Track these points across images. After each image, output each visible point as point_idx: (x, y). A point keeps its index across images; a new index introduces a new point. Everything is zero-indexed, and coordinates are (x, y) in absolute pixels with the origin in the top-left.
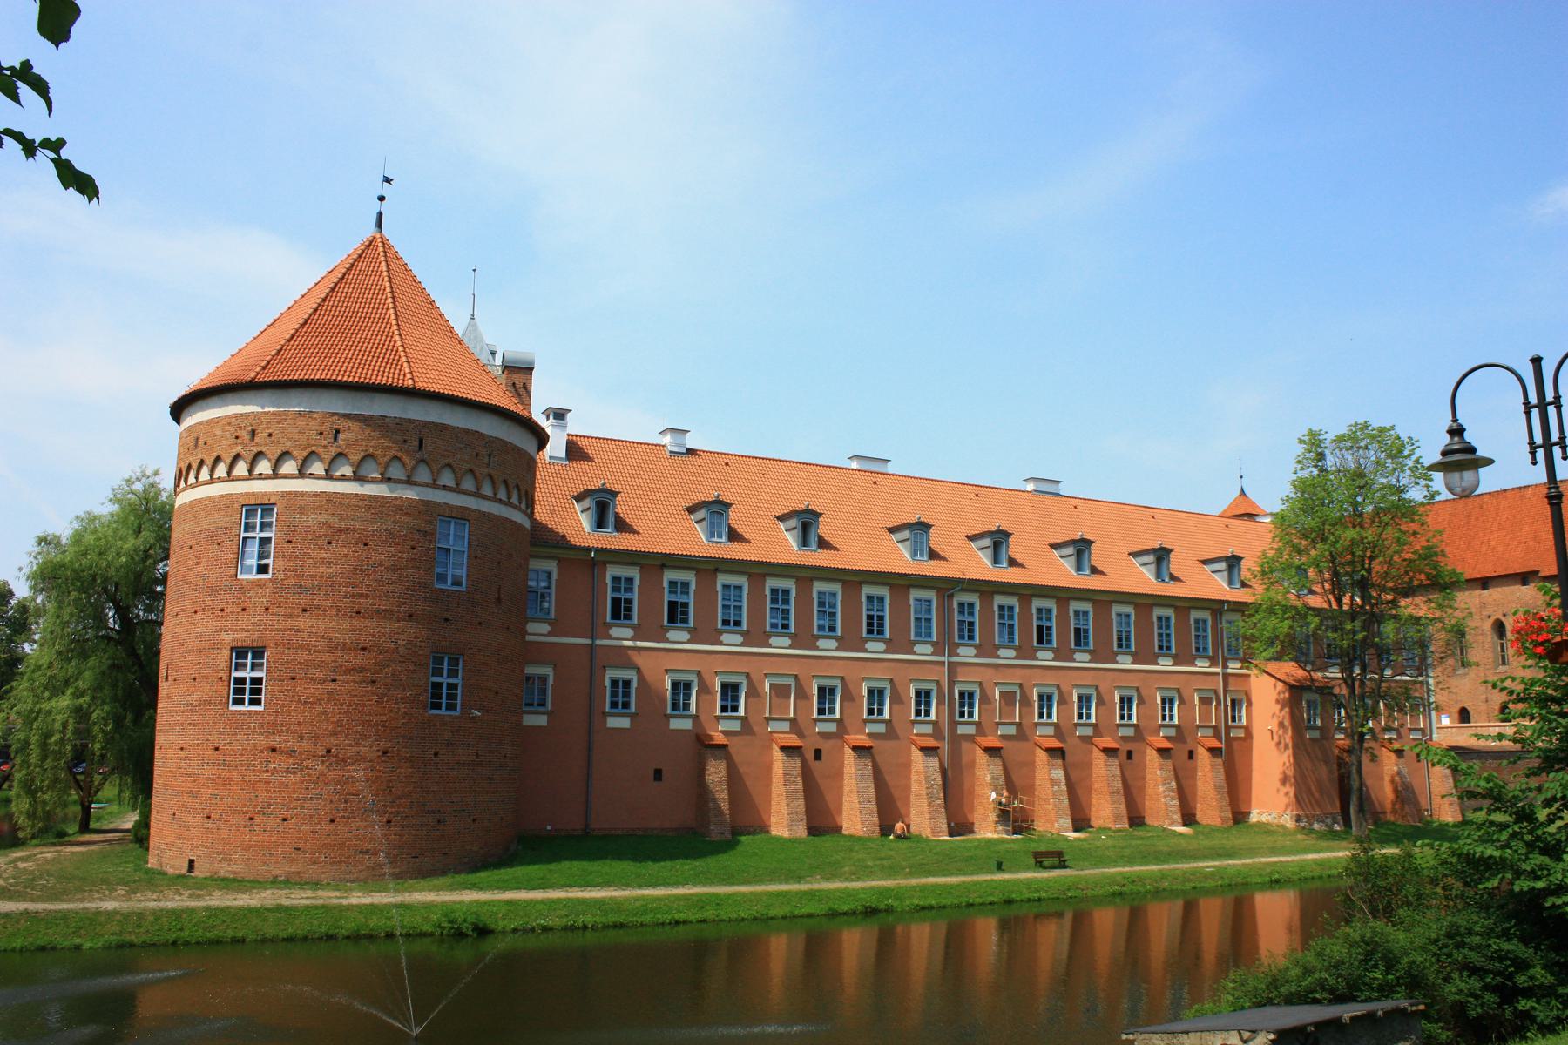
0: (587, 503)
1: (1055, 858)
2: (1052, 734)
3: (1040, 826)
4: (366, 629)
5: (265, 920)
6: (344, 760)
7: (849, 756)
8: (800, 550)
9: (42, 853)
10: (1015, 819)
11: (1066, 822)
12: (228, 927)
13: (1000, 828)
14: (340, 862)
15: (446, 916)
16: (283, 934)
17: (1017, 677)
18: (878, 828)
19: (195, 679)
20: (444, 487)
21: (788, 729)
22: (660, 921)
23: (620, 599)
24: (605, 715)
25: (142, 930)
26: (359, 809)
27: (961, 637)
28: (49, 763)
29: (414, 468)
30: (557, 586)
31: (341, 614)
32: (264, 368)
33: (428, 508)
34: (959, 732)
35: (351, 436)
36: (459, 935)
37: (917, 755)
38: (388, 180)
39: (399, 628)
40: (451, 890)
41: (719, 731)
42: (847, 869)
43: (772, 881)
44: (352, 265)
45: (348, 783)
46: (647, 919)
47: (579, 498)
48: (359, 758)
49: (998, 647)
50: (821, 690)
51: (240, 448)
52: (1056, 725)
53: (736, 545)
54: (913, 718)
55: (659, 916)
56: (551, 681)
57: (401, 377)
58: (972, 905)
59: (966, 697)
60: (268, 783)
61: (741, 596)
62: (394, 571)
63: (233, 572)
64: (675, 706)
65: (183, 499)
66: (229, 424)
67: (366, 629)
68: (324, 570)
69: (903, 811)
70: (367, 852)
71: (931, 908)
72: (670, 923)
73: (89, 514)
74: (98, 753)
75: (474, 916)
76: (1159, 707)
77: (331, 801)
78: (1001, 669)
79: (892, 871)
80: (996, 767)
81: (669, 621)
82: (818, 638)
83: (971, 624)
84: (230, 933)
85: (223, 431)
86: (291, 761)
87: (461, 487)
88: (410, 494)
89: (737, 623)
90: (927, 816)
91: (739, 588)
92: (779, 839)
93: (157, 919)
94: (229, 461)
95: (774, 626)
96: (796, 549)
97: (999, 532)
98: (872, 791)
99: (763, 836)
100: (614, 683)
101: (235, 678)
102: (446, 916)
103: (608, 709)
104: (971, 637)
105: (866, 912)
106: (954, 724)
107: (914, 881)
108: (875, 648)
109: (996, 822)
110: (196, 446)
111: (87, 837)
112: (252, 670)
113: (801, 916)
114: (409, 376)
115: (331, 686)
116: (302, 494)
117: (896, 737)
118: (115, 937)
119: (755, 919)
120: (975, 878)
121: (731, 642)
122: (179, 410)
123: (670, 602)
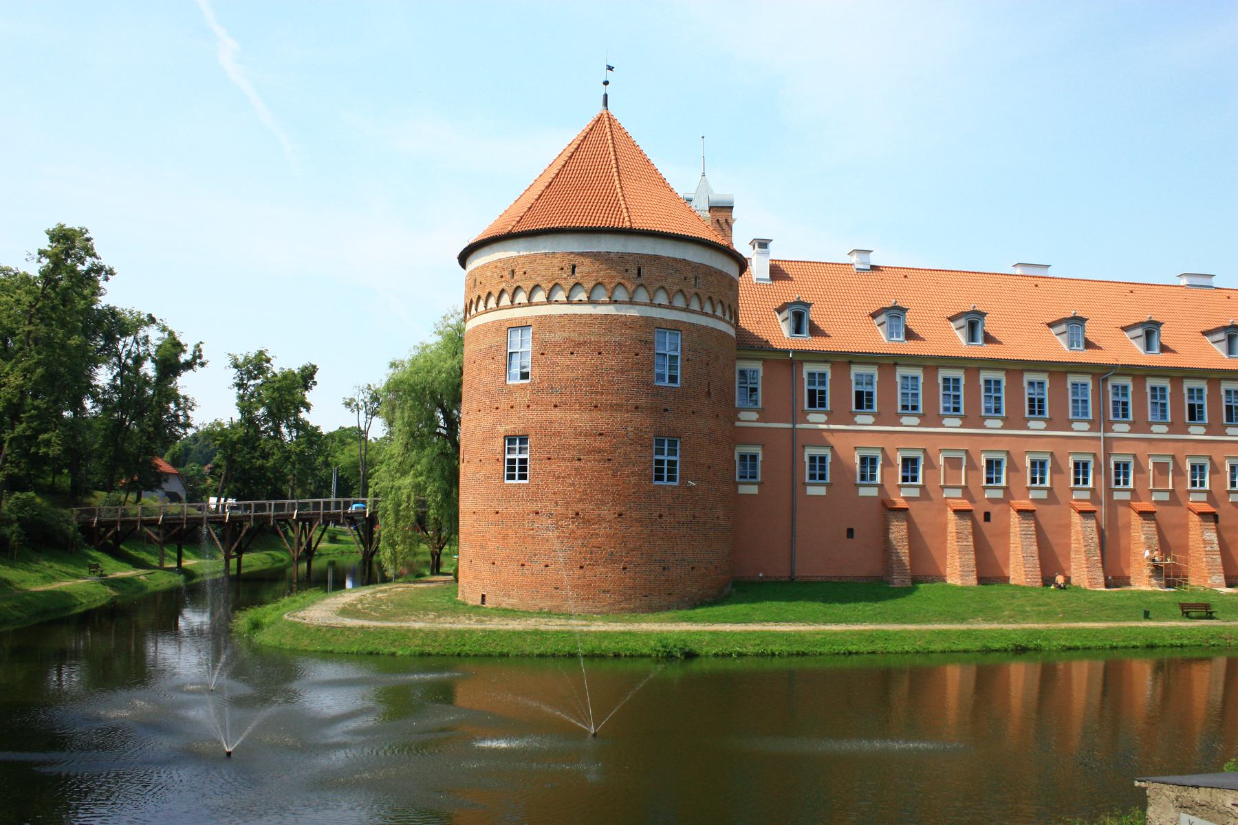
0: (786, 313)
1: (1206, 611)
2: (1205, 499)
3: (1193, 581)
4: (603, 419)
5: (525, 640)
6: (588, 521)
7: (1015, 518)
8: (968, 345)
9: (397, 588)
10: (1170, 575)
11: (1220, 579)
12: (497, 644)
13: (1154, 581)
14: (588, 599)
15: (661, 641)
16: (536, 652)
17: (1170, 449)
18: (1040, 580)
19: (481, 461)
20: (660, 305)
21: (961, 496)
22: (836, 651)
23: (1194, 404)
24: (805, 484)
25: (437, 644)
26: (601, 558)
27: (1116, 415)
28: (401, 524)
29: (634, 291)
30: (762, 382)
31: (583, 408)
32: (518, 222)
33: (647, 322)
34: (1115, 498)
36: (670, 657)
37: (1076, 518)
38: (610, 68)
39: (628, 417)
40: (672, 622)
41: (902, 495)
42: (1006, 613)
43: (938, 621)
44: (585, 137)
45: (592, 538)
46: (825, 649)
47: (780, 310)
49: (1151, 424)
50: (989, 462)
51: (504, 284)
52: (1209, 492)
53: (912, 343)
54: (1228, 488)
55: (835, 647)
56: (760, 458)
57: (621, 220)
58: (1116, 648)
59: (1122, 468)
60: (534, 538)
61: (917, 385)
62: (623, 373)
63: (503, 379)
64: (863, 477)
65: (470, 325)
66: (496, 267)
67: (603, 419)
68: (569, 374)
69: (1064, 566)
70: (609, 591)
71: (1076, 648)
72: (844, 654)
73: (422, 343)
74: (432, 517)
75: (682, 643)
76: (1072, 472)
77: (580, 552)
78: (835, 434)
79: (1047, 616)
80: (1151, 528)
81: (1190, 419)
82: (985, 418)
83: (1125, 404)
84: (499, 649)
85: (492, 272)
87: (673, 304)
88: (633, 312)
89: (915, 408)
90: (1085, 570)
91: (915, 378)
92: (953, 587)
93: (447, 637)
94: (497, 295)
95: (946, 409)
96: (965, 344)
97: (1151, 322)
98: (1035, 548)
99: (940, 584)
100: (812, 459)
101: (508, 459)
102: (661, 641)
104: (1125, 416)
105: (1017, 650)
106: (1110, 492)
107: (1064, 625)
108: (1037, 426)
109: (1150, 577)
110: (475, 286)
111: (436, 578)
112: (520, 453)
113: (958, 651)
114: (627, 219)
115: (577, 464)
116: (550, 316)
117: (929, 498)
118: (417, 648)
119: (918, 652)
120: (1121, 624)
121: (910, 423)
122: (463, 258)
123: (1189, 405)
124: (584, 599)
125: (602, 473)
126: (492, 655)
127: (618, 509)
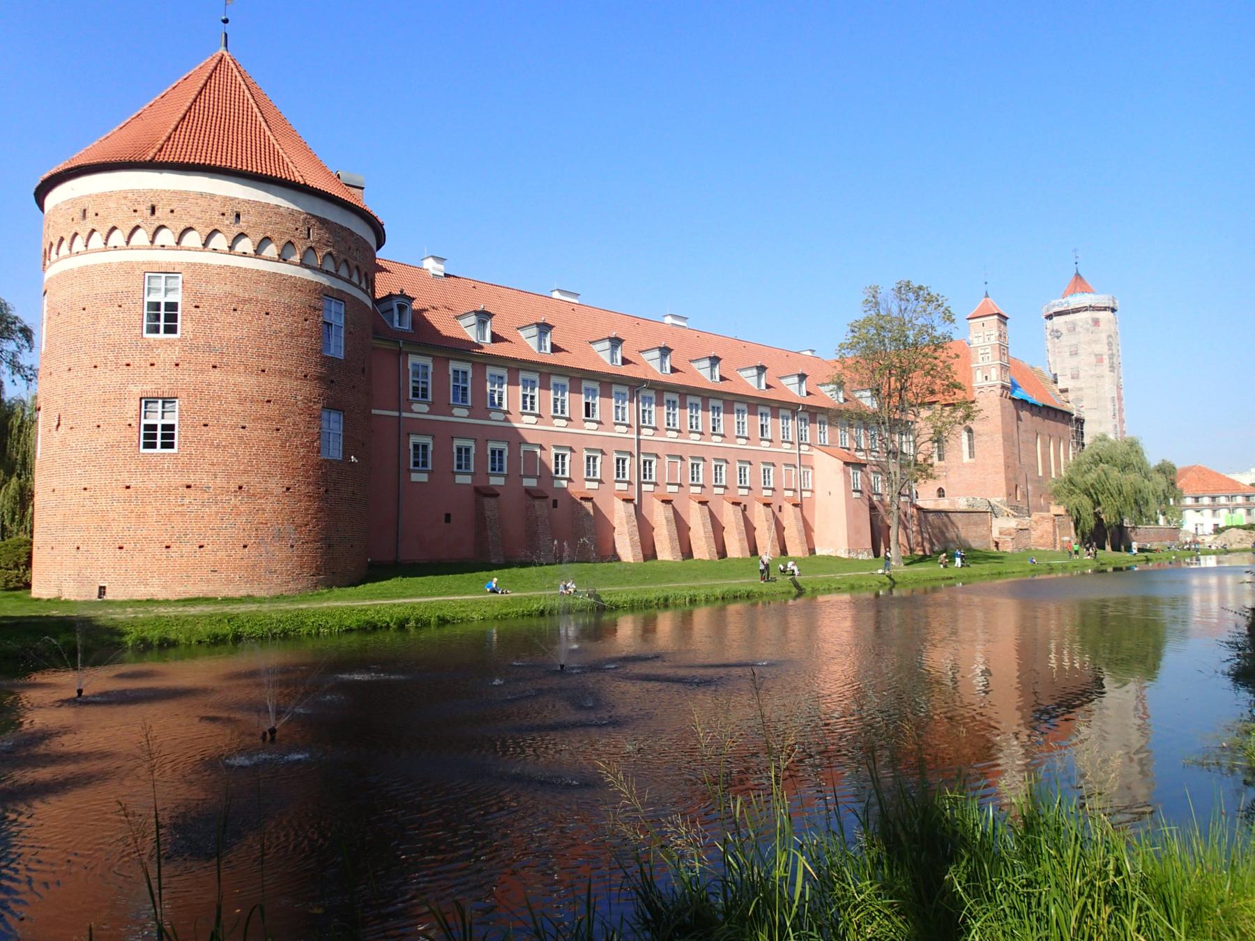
6: (254, 495)
24: (409, 471)
35: (253, 219)
39: (297, 385)
48: (267, 493)
86: (206, 496)
100: (416, 447)
103: (411, 467)
124: (247, 582)
125: (270, 443)
126: (173, 644)
127: (287, 483)
